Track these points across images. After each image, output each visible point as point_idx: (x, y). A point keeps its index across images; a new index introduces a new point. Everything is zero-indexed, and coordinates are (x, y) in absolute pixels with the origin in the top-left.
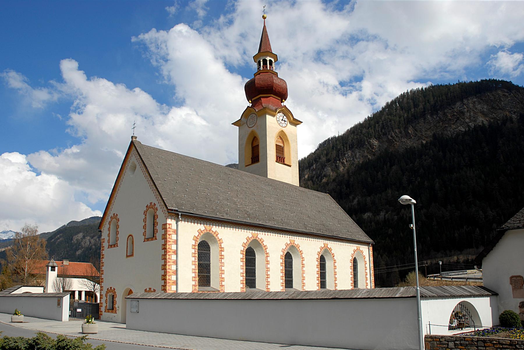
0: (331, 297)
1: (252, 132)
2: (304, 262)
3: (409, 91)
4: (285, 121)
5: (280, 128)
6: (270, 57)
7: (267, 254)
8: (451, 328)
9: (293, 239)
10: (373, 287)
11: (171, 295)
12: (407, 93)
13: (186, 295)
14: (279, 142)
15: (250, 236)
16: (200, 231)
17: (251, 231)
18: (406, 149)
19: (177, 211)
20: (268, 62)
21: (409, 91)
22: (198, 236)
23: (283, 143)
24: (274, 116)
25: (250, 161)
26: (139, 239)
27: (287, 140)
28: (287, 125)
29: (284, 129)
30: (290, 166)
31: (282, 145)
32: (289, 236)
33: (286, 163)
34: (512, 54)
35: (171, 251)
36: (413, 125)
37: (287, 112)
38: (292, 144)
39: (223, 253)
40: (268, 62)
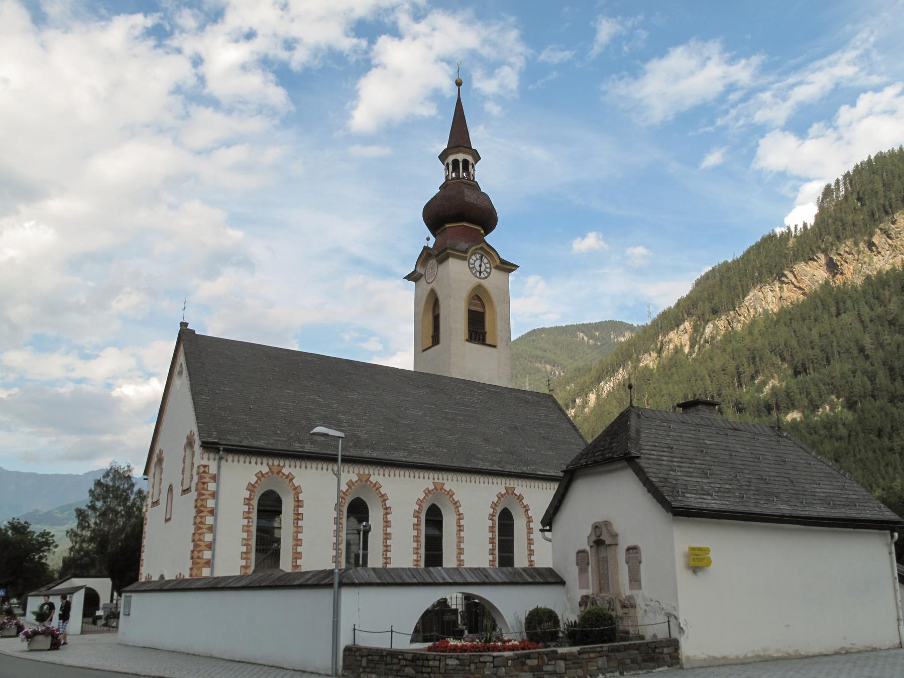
0: (240, 585)
1: (480, 287)
2: (462, 522)
3: (872, 158)
4: (480, 273)
5: (475, 281)
6: (464, 153)
7: (456, 503)
8: (412, 641)
9: (441, 481)
10: (422, 564)
11: (313, 576)
12: (869, 160)
13: (307, 577)
14: (476, 305)
15: (355, 478)
16: (260, 476)
17: (356, 471)
18: (868, 277)
19: (217, 443)
20: (461, 164)
21: (872, 158)
22: (256, 482)
23: (483, 306)
24: (464, 259)
25: (429, 342)
26: (177, 490)
27: (490, 301)
28: (489, 274)
29: (485, 283)
30: (494, 346)
31: (480, 310)
32: (431, 475)
33: (487, 342)
34: (837, 85)
35: (206, 510)
36: (881, 225)
37: (489, 252)
38: (499, 309)
39: (301, 510)
40: (461, 164)
